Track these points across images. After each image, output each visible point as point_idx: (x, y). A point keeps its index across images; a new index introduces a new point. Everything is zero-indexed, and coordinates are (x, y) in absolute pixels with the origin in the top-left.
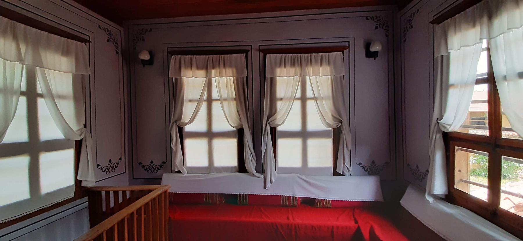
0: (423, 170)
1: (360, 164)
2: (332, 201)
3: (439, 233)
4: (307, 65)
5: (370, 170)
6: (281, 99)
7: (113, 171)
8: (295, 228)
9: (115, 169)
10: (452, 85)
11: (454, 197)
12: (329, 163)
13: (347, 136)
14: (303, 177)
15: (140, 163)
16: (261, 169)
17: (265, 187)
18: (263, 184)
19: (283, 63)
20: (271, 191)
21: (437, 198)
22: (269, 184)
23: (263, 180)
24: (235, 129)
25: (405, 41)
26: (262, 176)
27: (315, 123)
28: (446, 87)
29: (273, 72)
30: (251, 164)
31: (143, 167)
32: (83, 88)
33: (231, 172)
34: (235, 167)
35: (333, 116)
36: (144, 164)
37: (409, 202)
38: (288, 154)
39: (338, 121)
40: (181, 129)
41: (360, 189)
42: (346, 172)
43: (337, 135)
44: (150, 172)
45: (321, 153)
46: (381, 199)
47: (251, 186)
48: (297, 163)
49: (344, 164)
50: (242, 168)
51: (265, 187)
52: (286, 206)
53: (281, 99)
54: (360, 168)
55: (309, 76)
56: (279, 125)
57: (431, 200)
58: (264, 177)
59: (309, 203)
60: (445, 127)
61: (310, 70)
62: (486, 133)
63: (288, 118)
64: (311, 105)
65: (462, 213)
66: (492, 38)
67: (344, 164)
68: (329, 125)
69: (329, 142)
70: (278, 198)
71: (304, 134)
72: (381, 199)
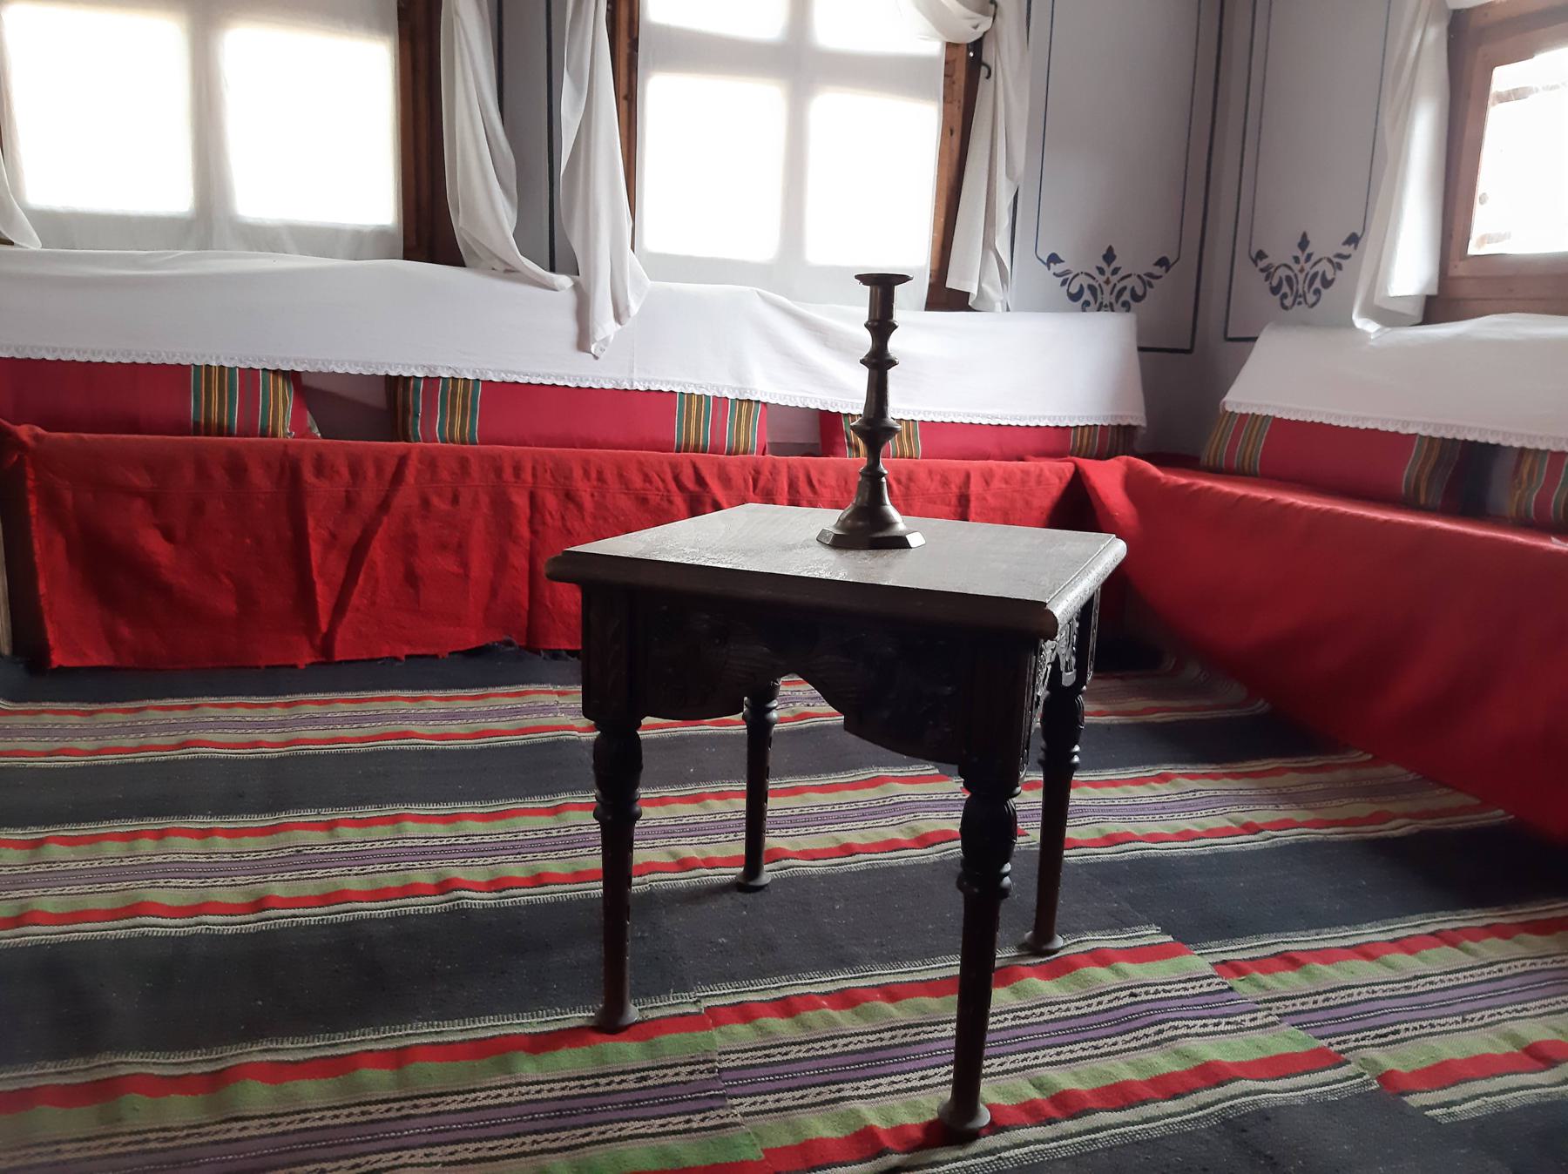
0: (1325, 244)
1: (1054, 259)
3: (1406, 424)
5: (1086, 294)
7: (1311, 298)
9: (1317, 292)
13: (1009, 94)
15: (1261, 255)
16: (553, 246)
17: (583, 341)
18: (570, 327)
20: (619, 363)
21: (1388, 317)
22: (605, 326)
26: (564, 281)
30: (484, 197)
32: (1409, 105)
34: (381, 234)
36: (1273, 258)
41: (1024, 365)
42: (994, 293)
44: (1288, 302)
45: (878, 178)
46: (1135, 415)
47: (486, 331)
49: (988, 244)
50: (428, 230)
51: (583, 341)
54: (1047, 279)
67: (988, 244)
69: (920, 123)
70: (177, 375)
72: (1135, 415)
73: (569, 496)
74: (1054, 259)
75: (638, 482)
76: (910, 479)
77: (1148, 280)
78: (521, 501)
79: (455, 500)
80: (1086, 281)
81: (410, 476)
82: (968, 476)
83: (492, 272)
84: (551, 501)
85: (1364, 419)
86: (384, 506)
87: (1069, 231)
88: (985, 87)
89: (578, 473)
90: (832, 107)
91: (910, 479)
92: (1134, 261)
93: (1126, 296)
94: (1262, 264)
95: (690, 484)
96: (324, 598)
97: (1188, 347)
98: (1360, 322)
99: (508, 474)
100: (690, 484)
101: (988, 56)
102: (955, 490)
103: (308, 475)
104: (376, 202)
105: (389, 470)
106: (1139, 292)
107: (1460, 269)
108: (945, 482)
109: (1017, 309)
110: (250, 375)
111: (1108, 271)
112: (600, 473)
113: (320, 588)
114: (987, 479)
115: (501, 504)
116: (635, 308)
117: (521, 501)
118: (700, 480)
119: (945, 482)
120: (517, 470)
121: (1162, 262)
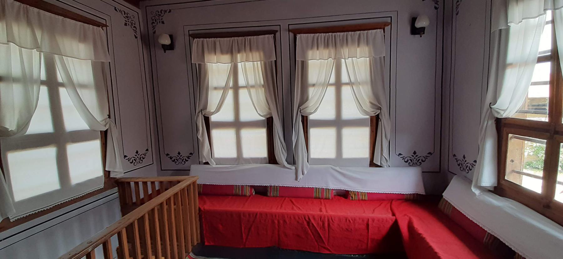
0: (470, 160)
1: (400, 154)
2: (369, 194)
4: (342, 46)
5: (412, 160)
6: (314, 85)
8: (328, 220)
10: (511, 64)
11: (503, 189)
12: (365, 153)
13: (385, 123)
14: (337, 168)
16: (292, 161)
17: (296, 179)
18: (294, 176)
19: (315, 45)
20: (303, 182)
22: (300, 176)
23: (294, 171)
24: (264, 118)
25: (457, 14)
26: (294, 168)
27: (351, 111)
28: (502, 66)
29: (304, 54)
30: (281, 155)
31: (171, 158)
33: (257, 163)
34: (265, 158)
35: (371, 103)
37: (453, 195)
38: (321, 144)
39: (376, 108)
40: (207, 120)
41: (400, 180)
42: (384, 164)
43: (375, 123)
45: (357, 142)
47: (282, 177)
48: (331, 154)
49: (382, 154)
50: (272, 159)
51: (296, 179)
52: (237, 195)
53: (314, 85)
54: (399, 159)
55: (345, 59)
56: (311, 113)
57: (477, 192)
58: (296, 168)
59: (344, 195)
60: (498, 113)
61: (345, 51)
62: (545, 119)
63: (321, 106)
64: (243, 93)
65: (510, 205)
66: (558, 9)
68: (366, 113)
70: (232, 186)
71: (338, 123)
72: (422, 192)
73: (285, 221)
74: (400, 154)
75: (297, 218)
76: (355, 220)
77: (426, 157)
78: (276, 222)
79: (265, 220)
80: (409, 158)
81: (258, 217)
82: (368, 220)
83: (281, 167)
84: (281, 222)
85: (474, 219)
86: (254, 222)
87: (405, 145)
88: (380, 123)
89: (286, 217)
90: (347, 132)
91: (355, 220)
92: (422, 153)
93: (420, 161)
94: (455, 157)
95: (307, 219)
96: (244, 236)
97: (438, 171)
98: (473, 189)
99: (274, 217)
100: (307, 219)
101: (380, 117)
102: (365, 222)
103: (242, 217)
104: (264, 153)
105: (255, 215)
106: (424, 160)
107: (503, 182)
108: (363, 221)
109: (392, 167)
110: (242, 186)
111: (415, 156)
112: (290, 217)
113: (244, 235)
114: (373, 220)
115: (273, 222)
116: (306, 172)
117: (276, 222)
118: (309, 219)
119: (363, 221)
120: (275, 216)
121: (429, 153)
